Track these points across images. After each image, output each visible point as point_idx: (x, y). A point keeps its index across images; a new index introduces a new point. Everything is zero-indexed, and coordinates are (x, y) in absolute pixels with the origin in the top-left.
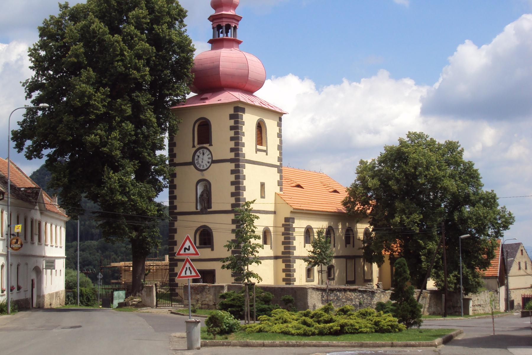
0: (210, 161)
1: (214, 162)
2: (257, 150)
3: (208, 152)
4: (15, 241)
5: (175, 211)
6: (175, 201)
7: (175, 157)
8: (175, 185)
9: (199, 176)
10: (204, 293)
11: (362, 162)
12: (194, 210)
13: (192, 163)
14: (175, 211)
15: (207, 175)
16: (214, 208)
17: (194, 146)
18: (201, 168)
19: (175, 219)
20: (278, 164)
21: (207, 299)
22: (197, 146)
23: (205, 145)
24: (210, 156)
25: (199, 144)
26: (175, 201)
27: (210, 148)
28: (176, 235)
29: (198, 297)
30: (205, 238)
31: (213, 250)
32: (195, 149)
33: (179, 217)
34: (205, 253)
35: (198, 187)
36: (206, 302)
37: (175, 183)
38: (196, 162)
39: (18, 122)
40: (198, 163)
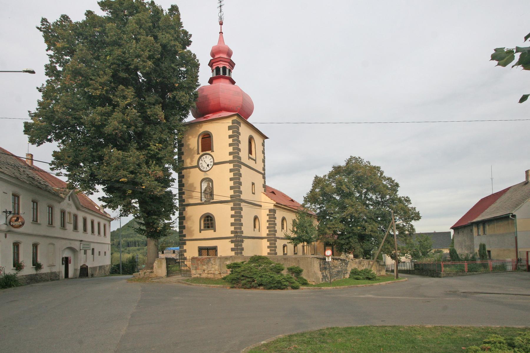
0: (212, 163)
1: (215, 164)
2: (250, 158)
3: (210, 157)
4: (15, 219)
5: (184, 203)
6: (183, 156)
7: (184, 186)
8: (183, 144)
9: (202, 176)
10: (210, 264)
11: (316, 177)
12: (200, 202)
13: (197, 166)
14: (184, 203)
15: (210, 175)
16: (216, 198)
17: (198, 154)
18: (205, 170)
19: (184, 210)
20: (263, 172)
21: (213, 269)
22: (201, 153)
23: (207, 152)
24: (212, 160)
25: (202, 151)
26: (183, 156)
27: (212, 153)
28: (184, 221)
29: (205, 267)
30: (209, 222)
31: (215, 231)
32: (199, 156)
33: (187, 242)
34: (209, 233)
35: (202, 184)
36: (212, 272)
37: (184, 215)
38: (200, 165)
39: (29, 112)
40: (202, 166)
